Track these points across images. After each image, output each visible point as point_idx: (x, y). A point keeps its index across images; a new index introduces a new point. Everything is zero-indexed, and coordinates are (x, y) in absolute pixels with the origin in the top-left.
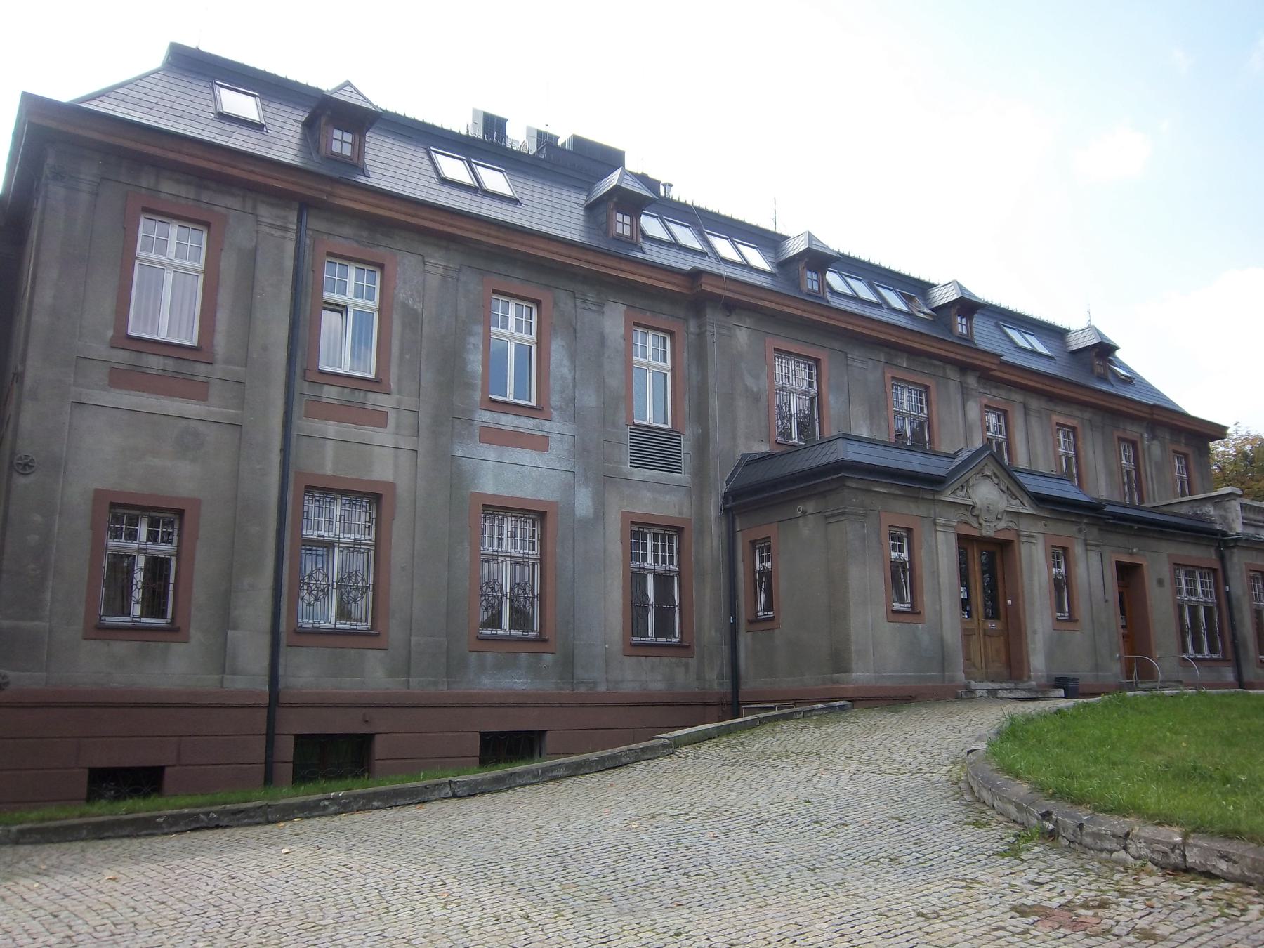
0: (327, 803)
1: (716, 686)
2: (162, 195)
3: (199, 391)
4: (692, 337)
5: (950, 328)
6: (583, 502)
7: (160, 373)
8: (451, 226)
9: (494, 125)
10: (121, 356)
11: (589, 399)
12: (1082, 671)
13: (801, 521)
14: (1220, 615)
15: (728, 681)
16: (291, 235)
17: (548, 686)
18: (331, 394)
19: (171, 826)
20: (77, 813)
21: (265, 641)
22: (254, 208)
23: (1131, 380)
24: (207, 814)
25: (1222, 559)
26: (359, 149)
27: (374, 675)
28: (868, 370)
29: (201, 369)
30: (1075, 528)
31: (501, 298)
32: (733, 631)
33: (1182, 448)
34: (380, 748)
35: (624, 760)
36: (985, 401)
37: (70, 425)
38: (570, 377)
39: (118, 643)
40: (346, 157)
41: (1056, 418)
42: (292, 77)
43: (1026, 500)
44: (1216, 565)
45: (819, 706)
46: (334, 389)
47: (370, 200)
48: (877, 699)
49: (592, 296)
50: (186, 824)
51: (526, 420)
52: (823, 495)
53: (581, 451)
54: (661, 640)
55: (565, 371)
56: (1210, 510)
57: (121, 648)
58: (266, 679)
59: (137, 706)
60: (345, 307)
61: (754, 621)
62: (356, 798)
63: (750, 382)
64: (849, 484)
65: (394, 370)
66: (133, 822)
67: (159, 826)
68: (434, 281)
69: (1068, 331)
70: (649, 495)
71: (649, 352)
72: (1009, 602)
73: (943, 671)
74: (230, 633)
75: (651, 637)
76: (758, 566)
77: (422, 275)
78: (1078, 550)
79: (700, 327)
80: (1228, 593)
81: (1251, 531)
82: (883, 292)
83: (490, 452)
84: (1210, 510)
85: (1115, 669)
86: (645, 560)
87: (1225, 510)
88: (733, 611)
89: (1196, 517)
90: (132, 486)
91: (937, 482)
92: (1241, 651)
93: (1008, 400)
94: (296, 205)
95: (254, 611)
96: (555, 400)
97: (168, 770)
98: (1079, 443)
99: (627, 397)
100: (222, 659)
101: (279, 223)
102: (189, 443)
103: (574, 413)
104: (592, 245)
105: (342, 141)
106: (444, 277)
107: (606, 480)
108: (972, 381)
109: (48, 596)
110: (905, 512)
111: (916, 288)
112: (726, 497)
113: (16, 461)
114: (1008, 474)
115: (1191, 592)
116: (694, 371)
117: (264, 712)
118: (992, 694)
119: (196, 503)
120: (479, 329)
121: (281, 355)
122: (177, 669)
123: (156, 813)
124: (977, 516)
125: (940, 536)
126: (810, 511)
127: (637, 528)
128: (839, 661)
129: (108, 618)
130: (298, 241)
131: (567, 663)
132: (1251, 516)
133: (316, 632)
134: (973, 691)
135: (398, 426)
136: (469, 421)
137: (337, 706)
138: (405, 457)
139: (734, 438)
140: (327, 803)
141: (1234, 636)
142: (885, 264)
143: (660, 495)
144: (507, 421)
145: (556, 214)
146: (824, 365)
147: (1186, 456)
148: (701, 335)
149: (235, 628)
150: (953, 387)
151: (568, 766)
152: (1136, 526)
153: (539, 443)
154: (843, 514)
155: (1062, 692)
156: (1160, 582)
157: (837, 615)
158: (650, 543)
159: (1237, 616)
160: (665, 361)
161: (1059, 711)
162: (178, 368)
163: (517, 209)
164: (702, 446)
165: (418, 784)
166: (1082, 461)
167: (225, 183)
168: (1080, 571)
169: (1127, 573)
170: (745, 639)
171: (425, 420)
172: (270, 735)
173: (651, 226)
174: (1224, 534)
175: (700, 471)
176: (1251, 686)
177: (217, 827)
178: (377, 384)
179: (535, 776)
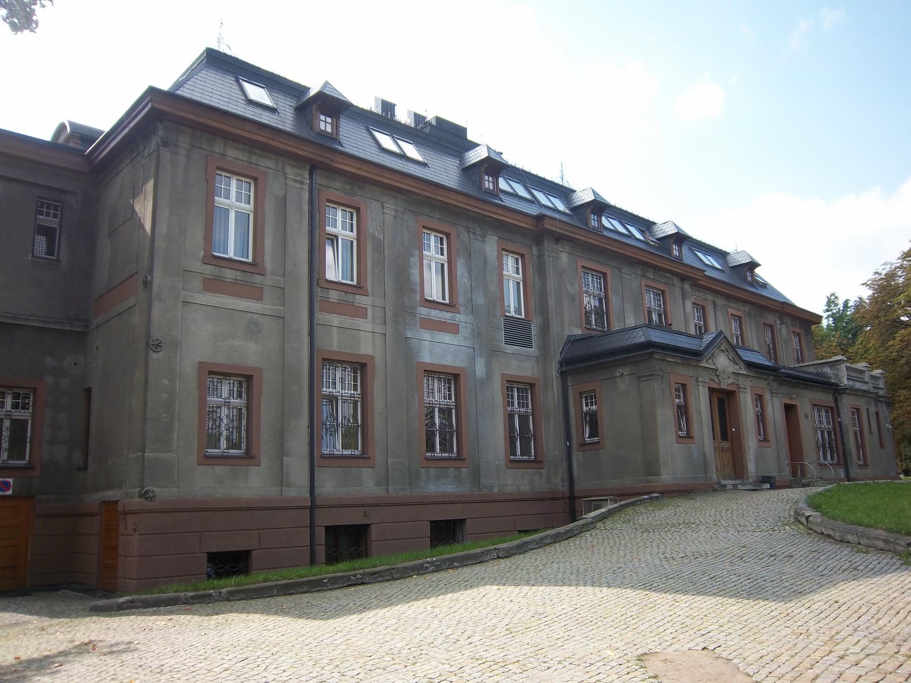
1: (560, 488)
2: (228, 158)
3: (256, 294)
4: (535, 258)
5: (669, 252)
6: (480, 368)
8: (401, 183)
9: (388, 107)
10: (209, 270)
11: (480, 299)
12: (773, 473)
13: (618, 380)
14: (835, 436)
15: (567, 484)
16: (306, 188)
17: (465, 489)
18: (334, 295)
19: (333, 584)
20: (260, 579)
21: (306, 464)
22: (283, 168)
23: (765, 285)
24: (355, 576)
25: (836, 401)
26: (336, 127)
27: (367, 484)
28: (632, 279)
29: (258, 279)
30: (765, 383)
31: (224, 174)
32: (569, 450)
33: (797, 330)
34: (374, 533)
35: (576, 532)
36: (693, 300)
38: (468, 285)
40: (328, 133)
41: (731, 311)
42: (282, 75)
43: (742, 366)
44: (833, 405)
45: (646, 497)
47: (519, 218)
48: (677, 491)
49: (479, 231)
51: (446, 313)
53: (477, 334)
54: (525, 458)
55: (466, 280)
56: (827, 370)
57: (220, 470)
58: (308, 489)
59: (233, 509)
60: (336, 237)
61: (583, 444)
62: (444, 561)
63: (569, 288)
64: (656, 356)
65: (369, 281)
66: (308, 583)
68: (389, 219)
69: (654, 224)
70: (515, 362)
71: (233, 194)
73: (706, 473)
75: (519, 457)
76: (585, 409)
77: (383, 213)
78: (767, 397)
79: (539, 252)
80: (840, 422)
81: (851, 383)
82: (536, 193)
83: (426, 335)
84: (827, 370)
85: (787, 472)
86: (513, 405)
88: (568, 437)
89: (818, 374)
90: (221, 359)
91: (697, 355)
92: (848, 458)
93: (705, 299)
94: (308, 167)
95: (298, 443)
96: (461, 300)
97: (254, 553)
98: (743, 327)
99: (501, 297)
100: (281, 476)
101: (299, 179)
102: (253, 331)
103: (473, 310)
104: (471, 197)
105: (326, 122)
106: (395, 217)
107: (492, 353)
108: (687, 287)
109: (175, 435)
110: (682, 373)
111: (646, 225)
112: (561, 364)
113: (151, 343)
114: (733, 350)
115: (821, 422)
116: (537, 280)
117: (308, 511)
118: (735, 487)
119: (260, 370)
120: (416, 252)
121: (305, 269)
122: (254, 484)
123: (322, 577)
124: (718, 376)
125: (701, 388)
126: (626, 373)
127: (510, 384)
128: (651, 467)
129: (209, 450)
130: (311, 192)
131: (476, 474)
132: (851, 374)
133: (332, 457)
134: (725, 486)
135: (373, 318)
136: (413, 314)
139: (563, 325)
141: (844, 450)
142: (541, 175)
143: (522, 363)
144: (436, 314)
145: (444, 171)
146: (609, 277)
147: (799, 335)
148: (541, 257)
149: (288, 456)
150: (677, 291)
151: (551, 536)
152: (794, 381)
153: (453, 329)
154: (652, 375)
155: (768, 486)
156: (806, 417)
157: (648, 439)
158: (516, 394)
159: (845, 437)
160: (518, 273)
161: (820, 493)
162: (245, 277)
163: (426, 170)
164: (545, 328)
165: (478, 550)
166: (745, 338)
167: (214, 133)
168: (769, 409)
169: (789, 409)
170: (577, 456)
171: (389, 314)
172: (312, 527)
173: (503, 184)
174: (837, 385)
175: (544, 348)
176: (855, 479)
177: (363, 584)
178: (360, 288)
179: (537, 544)
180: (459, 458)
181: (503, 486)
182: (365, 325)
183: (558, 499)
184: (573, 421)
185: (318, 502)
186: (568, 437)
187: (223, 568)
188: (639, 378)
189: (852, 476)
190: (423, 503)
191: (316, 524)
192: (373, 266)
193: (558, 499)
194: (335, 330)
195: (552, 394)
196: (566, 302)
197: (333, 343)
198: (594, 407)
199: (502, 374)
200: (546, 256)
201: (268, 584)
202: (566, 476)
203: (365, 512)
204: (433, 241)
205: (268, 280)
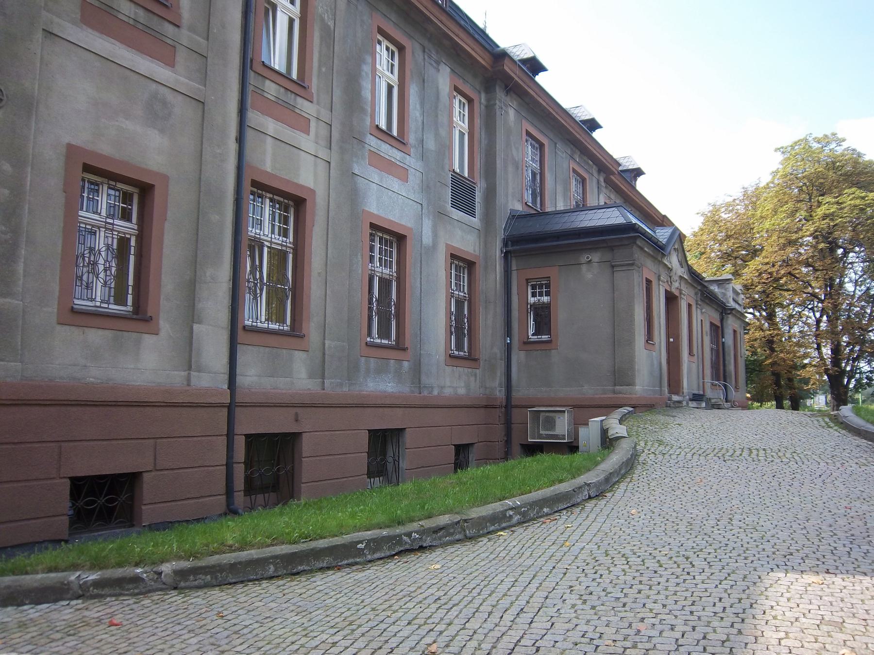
0: (511, 513)
7: (131, 22)
11: (431, 144)
13: (584, 268)
24: (409, 535)
27: (298, 375)
29: (169, 29)
32: (509, 347)
37: (42, 58)
39: (93, 330)
44: (719, 325)
46: (273, 85)
50: (390, 548)
52: (611, 248)
55: (418, 114)
57: (96, 336)
58: (227, 377)
59: (116, 404)
67: (360, 552)
70: (460, 233)
72: (671, 340)
74: (195, 326)
79: (488, 100)
83: (375, 175)
87: (726, 290)
88: (509, 332)
90: (105, 148)
96: (411, 138)
97: (146, 476)
100: (188, 354)
102: (157, 113)
112: (505, 243)
117: (225, 410)
119: (165, 178)
122: (145, 364)
128: (622, 375)
131: (417, 369)
135: (317, 136)
136: (361, 142)
137: (275, 406)
138: (322, 165)
140: (511, 513)
141: (724, 371)
149: (200, 322)
153: (401, 173)
157: (619, 341)
159: (727, 358)
170: (518, 356)
172: (230, 435)
177: (422, 548)
180: (399, 346)
181: (442, 387)
182: (307, 142)
183: (494, 407)
184: (515, 314)
185: (239, 398)
186: (509, 332)
187: (94, 502)
188: (613, 267)
189: (729, 398)
190: (363, 405)
191: (236, 431)
192: (320, 61)
193: (494, 407)
194: (269, 140)
195: (491, 279)
196: (510, 169)
197: (267, 161)
198: (545, 299)
199: (447, 245)
200: (497, 107)
201: (253, 553)
202: (503, 379)
203: (297, 414)
204: (382, 53)
205: (185, 36)
